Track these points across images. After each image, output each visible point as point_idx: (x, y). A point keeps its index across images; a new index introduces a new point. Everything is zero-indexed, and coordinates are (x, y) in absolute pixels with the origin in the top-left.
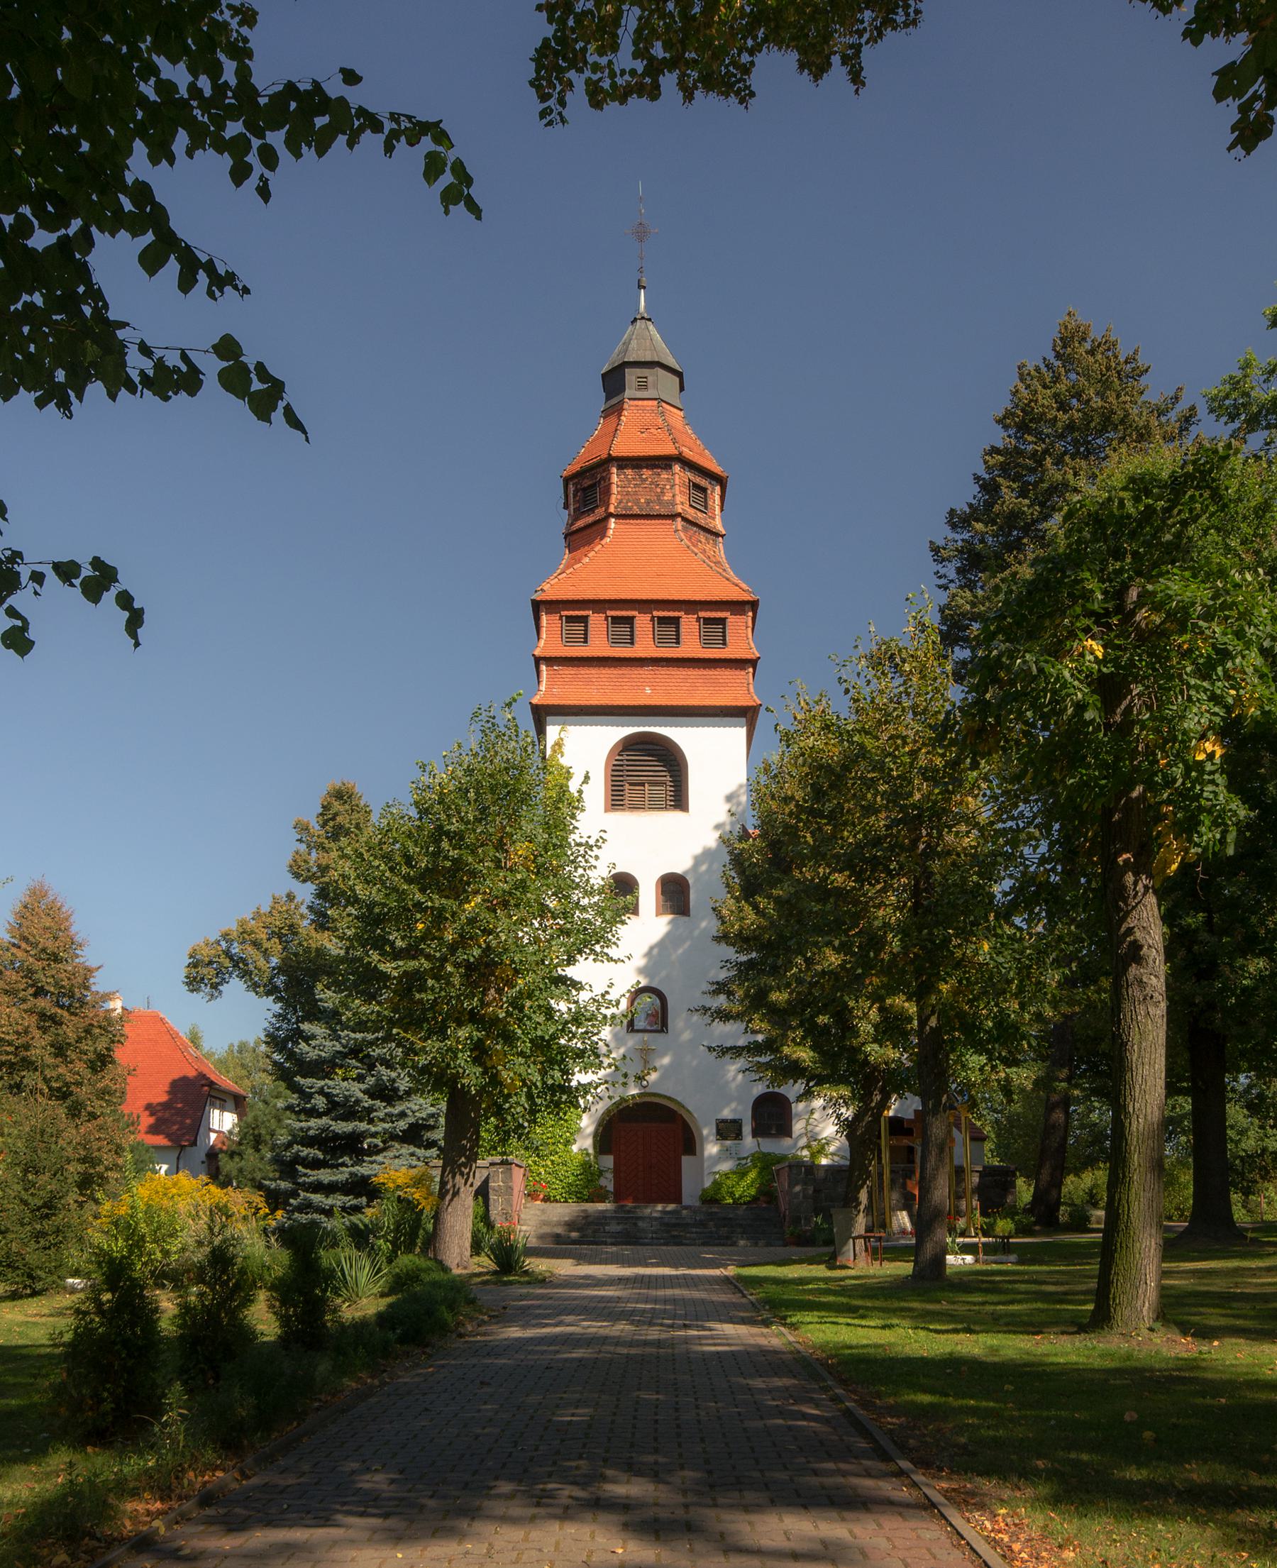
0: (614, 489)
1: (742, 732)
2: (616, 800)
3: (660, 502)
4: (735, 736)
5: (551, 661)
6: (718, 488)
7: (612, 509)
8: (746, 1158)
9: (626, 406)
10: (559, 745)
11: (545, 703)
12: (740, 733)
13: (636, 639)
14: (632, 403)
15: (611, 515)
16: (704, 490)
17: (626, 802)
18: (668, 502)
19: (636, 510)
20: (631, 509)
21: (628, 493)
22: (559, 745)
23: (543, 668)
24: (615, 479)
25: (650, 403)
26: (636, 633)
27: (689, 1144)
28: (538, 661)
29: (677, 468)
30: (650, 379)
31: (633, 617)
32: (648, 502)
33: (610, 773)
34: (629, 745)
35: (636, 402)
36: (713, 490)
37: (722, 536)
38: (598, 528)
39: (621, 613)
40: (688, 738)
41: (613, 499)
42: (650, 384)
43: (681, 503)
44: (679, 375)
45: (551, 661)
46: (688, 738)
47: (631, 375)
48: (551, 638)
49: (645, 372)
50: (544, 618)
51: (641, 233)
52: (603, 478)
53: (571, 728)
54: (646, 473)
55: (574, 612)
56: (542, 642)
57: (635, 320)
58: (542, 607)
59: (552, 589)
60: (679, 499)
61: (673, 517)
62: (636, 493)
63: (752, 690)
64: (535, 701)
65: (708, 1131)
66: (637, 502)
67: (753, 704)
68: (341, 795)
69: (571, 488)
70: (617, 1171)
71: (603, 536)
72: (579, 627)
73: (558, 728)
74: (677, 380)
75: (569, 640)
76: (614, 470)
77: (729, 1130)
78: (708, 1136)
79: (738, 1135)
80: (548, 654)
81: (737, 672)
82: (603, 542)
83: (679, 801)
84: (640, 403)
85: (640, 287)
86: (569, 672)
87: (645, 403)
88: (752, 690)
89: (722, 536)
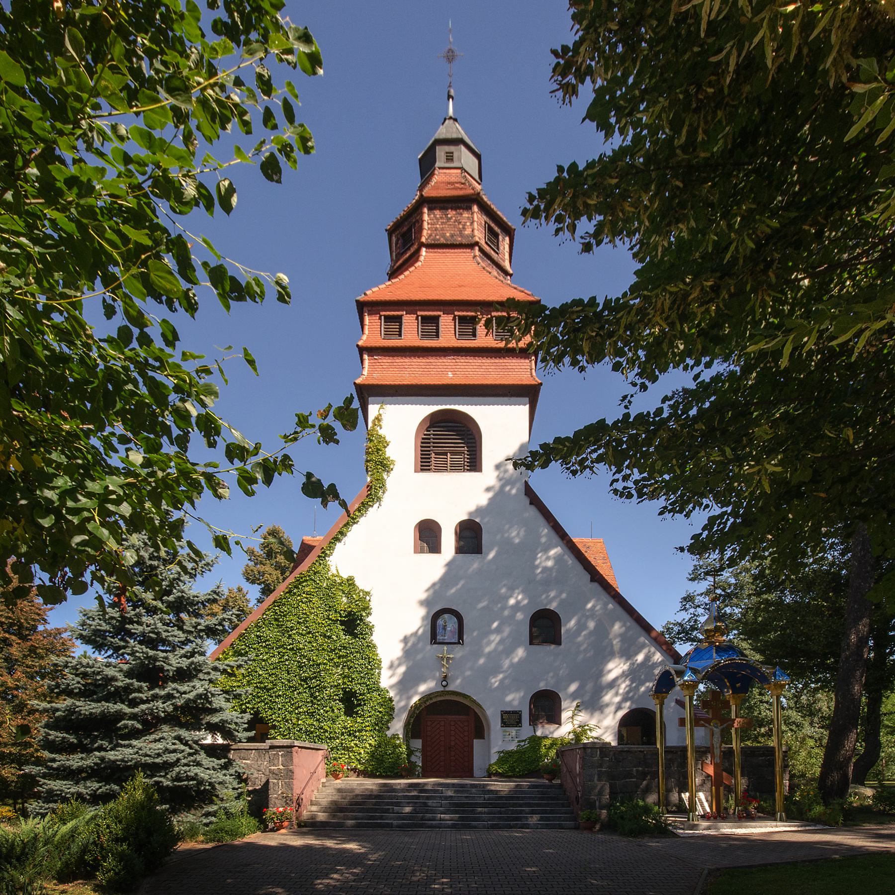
0: (426, 225)
1: (525, 409)
2: (424, 464)
3: (461, 235)
4: (519, 412)
5: (372, 351)
6: (507, 239)
7: (423, 240)
8: (525, 741)
9: (436, 172)
10: (378, 419)
11: (367, 383)
12: (523, 411)
13: (440, 334)
14: (441, 171)
15: (422, 245)
16: (496, 236)
17: (432, 467)
18: (468, 236)
19: (442, 241)
20: (439, 240)
21: (436, 229)
22: (378, 419)
23: (366, 357)
24: (426, 217)
25: (456, 171)
26: (441, 329)
27: (479, 730)
28: (362, 350)
29: (475, 208)
30: (455, 155)
31: (440, 316)
32: (452, 236)
33: (419, 444)
34: (435, 422)
35: (445, 171)
36: (504, 240)
37: (511, 275)
38: (415, 256)
39: (429, 311)
40: (483, 414)
41: (425, 233)
42: (455, 159)
43: (480, 235)
44: (478, 156)
45: (372, 351)
46: (483, 414)
47: (441, 151)
48: (373, 332)
49: (452, 148)
50: (367, 319)
51: (450, 57)
52: (417, 221)
53: (388, 407)
54: (451, 213)
55: (391, 311)
56: (365, 337)
57: (445, 120)
58: (365, 309)
59: (375, 293)
60: (476, 232)
61: (471, 246)
62: (442, 229)
63: (534, 374)
64: (358, 381)
65: (495, 724)
66: (444, 236)
67: (534, 383)
68: (274, 533)
69: (394, 239)
70: (424, 751)
71: (417, 260)
72: (394, 326)
73: (377, 407)
74: (476, 161)
75: (388, 334)
76: (426, 210)
77: (511, 719)
78: (615, 638)
79: (518, 723)
80: (369, 345)
81: (522, 361)
82: (416, 265)
83: (474, 464)
84: (448, 171)
85: (449, 97)
86: (386, 361)
87: (452, 171)
88: (534, 374)
89: (511, 275)
